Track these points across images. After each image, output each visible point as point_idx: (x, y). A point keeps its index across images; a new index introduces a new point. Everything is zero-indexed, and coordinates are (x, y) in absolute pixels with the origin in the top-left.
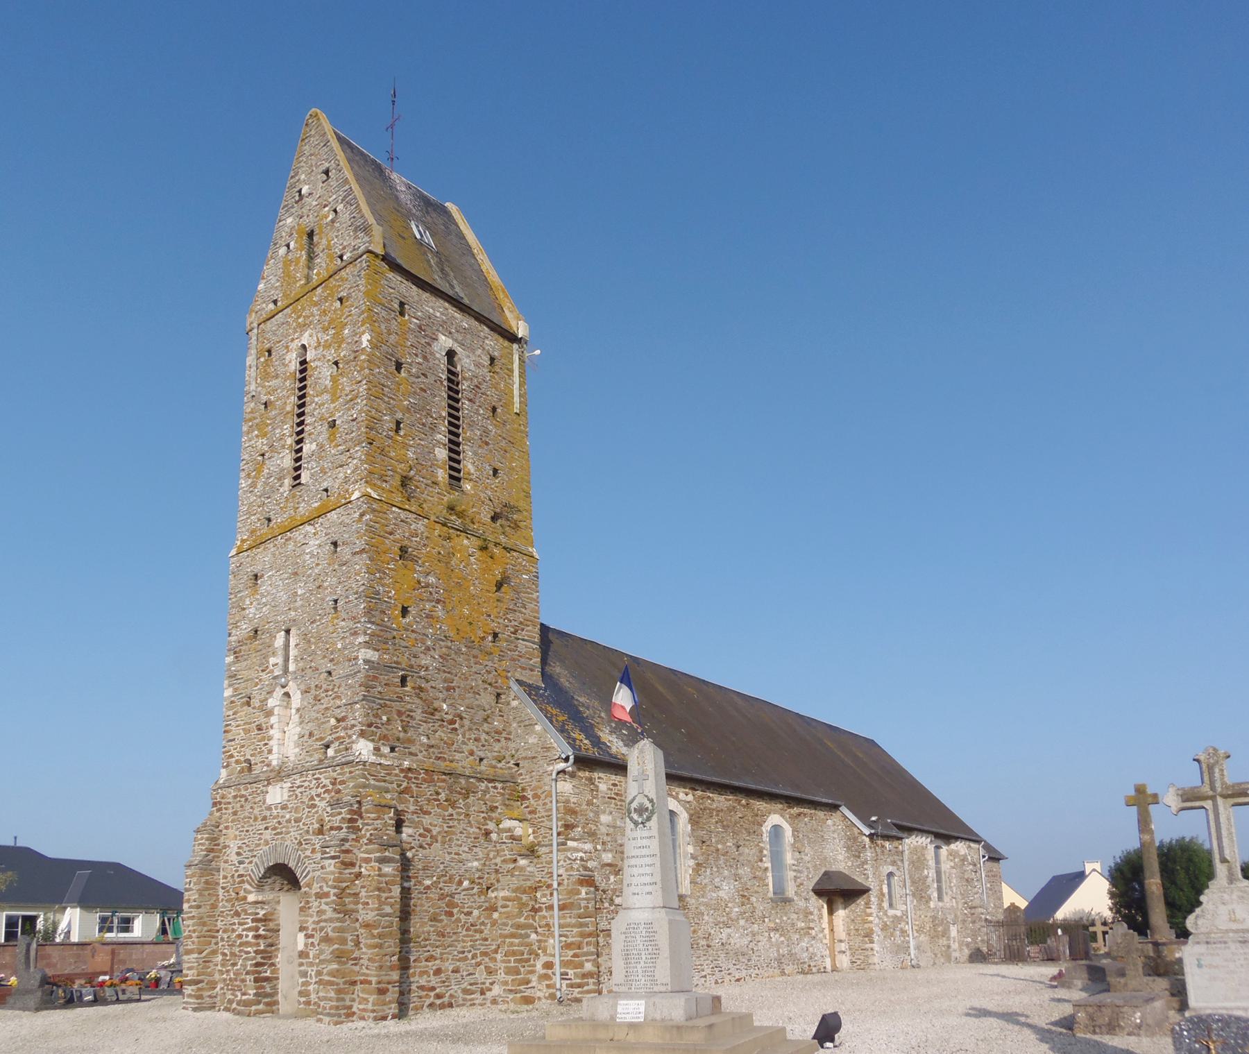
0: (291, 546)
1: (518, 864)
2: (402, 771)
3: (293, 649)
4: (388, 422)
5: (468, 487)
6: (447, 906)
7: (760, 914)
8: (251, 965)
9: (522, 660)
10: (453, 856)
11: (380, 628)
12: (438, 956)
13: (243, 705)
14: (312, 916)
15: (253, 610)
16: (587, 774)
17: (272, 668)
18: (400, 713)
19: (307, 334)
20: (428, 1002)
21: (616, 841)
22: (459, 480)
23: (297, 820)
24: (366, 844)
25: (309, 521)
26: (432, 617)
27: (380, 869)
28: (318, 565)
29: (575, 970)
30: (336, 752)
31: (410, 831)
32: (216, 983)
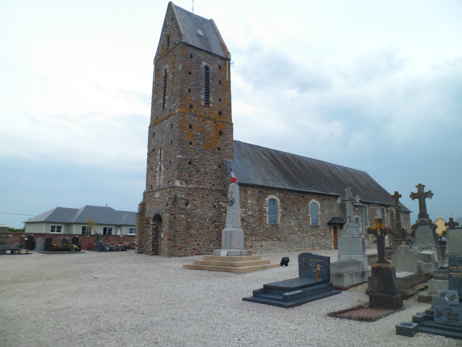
0: (162, 126)
1: (223, 215)
2: (188, 189)
4: (187, 90)
5: (211, 105)
6: (202, 226)
7: (306, 231)
8: (151, 241)
9: (227, 155)
10: (204, 212)
11: (182, 149)
12: (198, 240)
13: (151, 170)
15: (153, 143)
16: (244, 188)
18: (188, 172)
19: (167, 65)
20: (195, 253)
21: (253, 208)
22: (208, 104)
23: (162, 202)
25: (166, 119)
26: (199, 145)
27: (180, 216)
28: (168, 131)
30: (171, 183)
31: (191, 205)
32: (144, 246)
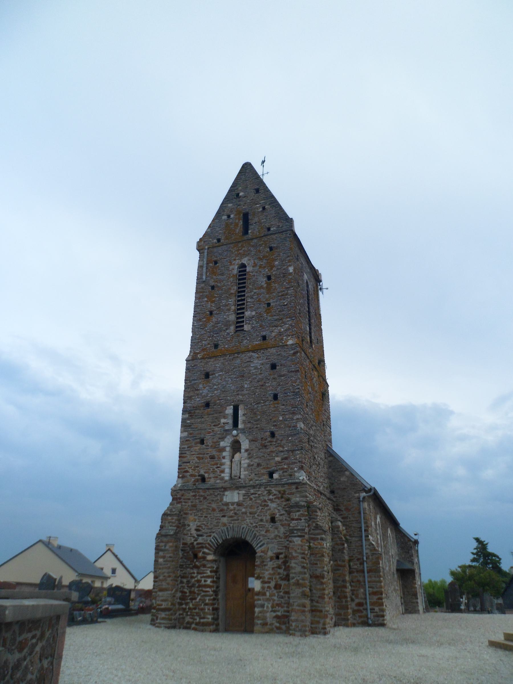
0: (238, 361)
3: (241, 417)
14: (267, 570)
17: (222, 424)
24: (313, 530)
29: (379, 607)
